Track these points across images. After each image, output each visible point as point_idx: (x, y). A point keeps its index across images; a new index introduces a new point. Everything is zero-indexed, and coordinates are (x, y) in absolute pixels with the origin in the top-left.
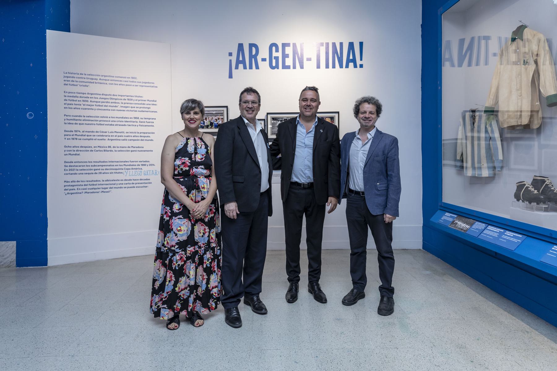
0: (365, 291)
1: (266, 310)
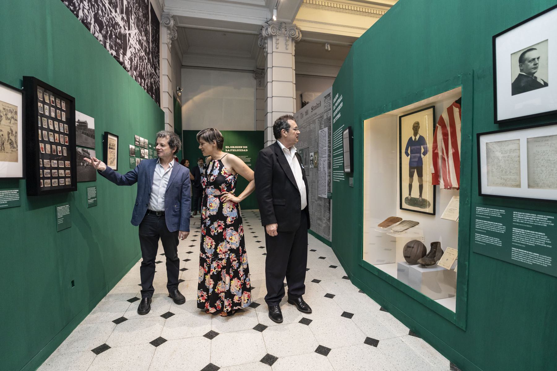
0: (365, 295)
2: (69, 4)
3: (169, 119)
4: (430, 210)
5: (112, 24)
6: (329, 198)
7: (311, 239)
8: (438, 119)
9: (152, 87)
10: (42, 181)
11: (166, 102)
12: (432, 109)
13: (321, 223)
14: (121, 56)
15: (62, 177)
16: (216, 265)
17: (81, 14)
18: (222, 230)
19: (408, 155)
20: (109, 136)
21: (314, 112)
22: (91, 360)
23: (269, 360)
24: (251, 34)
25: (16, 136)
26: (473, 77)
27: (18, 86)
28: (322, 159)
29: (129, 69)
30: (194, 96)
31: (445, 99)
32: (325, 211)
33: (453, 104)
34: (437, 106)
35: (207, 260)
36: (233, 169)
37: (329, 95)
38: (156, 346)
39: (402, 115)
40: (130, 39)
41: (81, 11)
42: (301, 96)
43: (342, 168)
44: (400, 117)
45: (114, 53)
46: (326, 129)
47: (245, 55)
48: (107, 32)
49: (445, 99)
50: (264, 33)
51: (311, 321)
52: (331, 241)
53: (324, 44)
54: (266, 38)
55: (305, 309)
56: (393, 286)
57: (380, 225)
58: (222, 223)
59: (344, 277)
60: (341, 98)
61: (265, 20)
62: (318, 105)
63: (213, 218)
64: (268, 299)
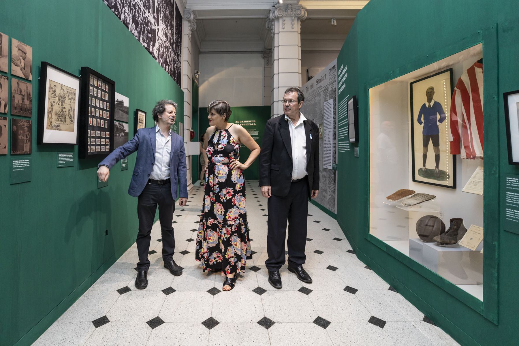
0: (372, 271)
1: (311, 279)
2: (115, 10)
3: (188, 98)
4: (449, 182)
5: (145, 23)
6: (334, 170)
7: (312, 209)
8: (456, 82)
9: (174, 71)
10: (89, 147)
11: (186, 84)
12: (448, 73)
13: (326, 195)
14: (151, 47)
15: (103, 145)
16: (225, 232)
17: (122, 17)
18: (230, 197)
19: (420, 123)
20: (139, 113)
21: (319, 85)
22: (116, 299)
23: (266, 323)
24: (260, 18)
25: (74, 112)
26: (497, 30)
27: (77, 74)
28: (327, 131)
29: (157, 57)
30: (210, 77)
31: (464, 59)
32: (330, 182)
33: (475, 65)
34: (455, 69)
35: (219, 225)
36: (239, 139)
37: (334, 67)
38: (167, 294)
39: (414, 80)
40: (159, 33)
41: (123, 15)
42: (308, 71)
43: (348, 138)
44: (411, 84)
45: (146, 45)
46: (331, 101)
47: (253, 37)
48: (141, 29)
49: (464, 59)
50: (271, 16)
51: (311, 291)
52: (336, 213)
53: (330, 20)
54: (273, 20)
55: (305, 278)
56: (403, 263)
57: (389, 198)
58: (231, 189)
59: (349, 251)
60: (346, 69)
61: (273, 4)
62: (323, 78)
63: (222, 185)
64: (268, 264)
